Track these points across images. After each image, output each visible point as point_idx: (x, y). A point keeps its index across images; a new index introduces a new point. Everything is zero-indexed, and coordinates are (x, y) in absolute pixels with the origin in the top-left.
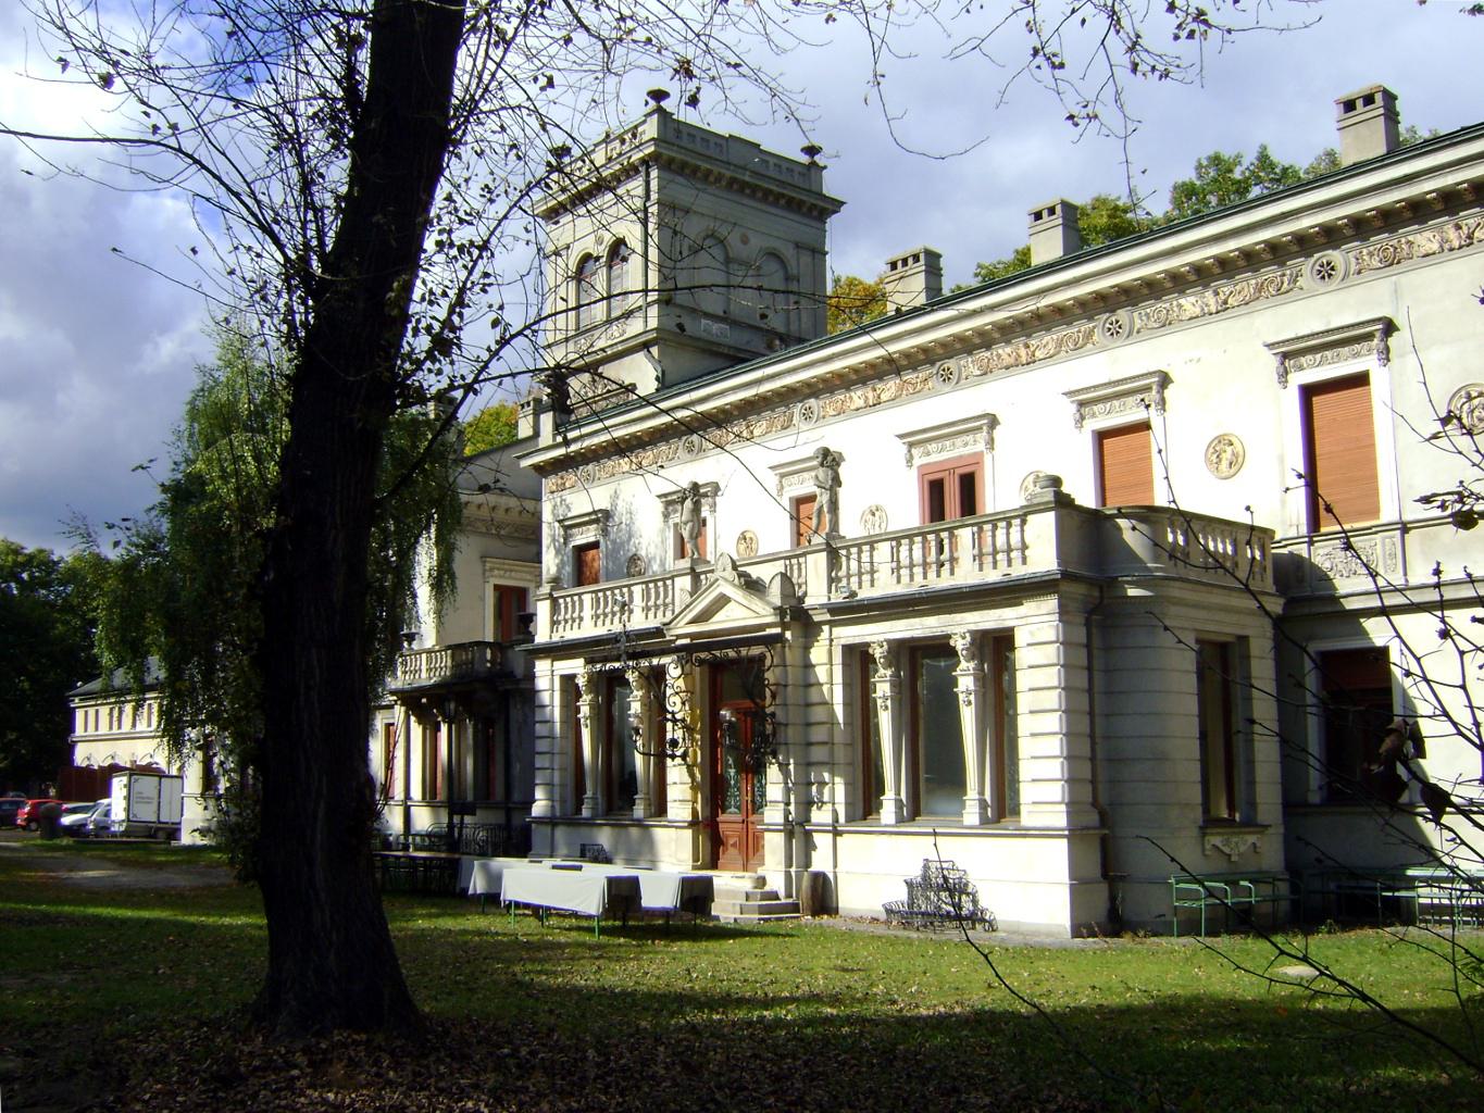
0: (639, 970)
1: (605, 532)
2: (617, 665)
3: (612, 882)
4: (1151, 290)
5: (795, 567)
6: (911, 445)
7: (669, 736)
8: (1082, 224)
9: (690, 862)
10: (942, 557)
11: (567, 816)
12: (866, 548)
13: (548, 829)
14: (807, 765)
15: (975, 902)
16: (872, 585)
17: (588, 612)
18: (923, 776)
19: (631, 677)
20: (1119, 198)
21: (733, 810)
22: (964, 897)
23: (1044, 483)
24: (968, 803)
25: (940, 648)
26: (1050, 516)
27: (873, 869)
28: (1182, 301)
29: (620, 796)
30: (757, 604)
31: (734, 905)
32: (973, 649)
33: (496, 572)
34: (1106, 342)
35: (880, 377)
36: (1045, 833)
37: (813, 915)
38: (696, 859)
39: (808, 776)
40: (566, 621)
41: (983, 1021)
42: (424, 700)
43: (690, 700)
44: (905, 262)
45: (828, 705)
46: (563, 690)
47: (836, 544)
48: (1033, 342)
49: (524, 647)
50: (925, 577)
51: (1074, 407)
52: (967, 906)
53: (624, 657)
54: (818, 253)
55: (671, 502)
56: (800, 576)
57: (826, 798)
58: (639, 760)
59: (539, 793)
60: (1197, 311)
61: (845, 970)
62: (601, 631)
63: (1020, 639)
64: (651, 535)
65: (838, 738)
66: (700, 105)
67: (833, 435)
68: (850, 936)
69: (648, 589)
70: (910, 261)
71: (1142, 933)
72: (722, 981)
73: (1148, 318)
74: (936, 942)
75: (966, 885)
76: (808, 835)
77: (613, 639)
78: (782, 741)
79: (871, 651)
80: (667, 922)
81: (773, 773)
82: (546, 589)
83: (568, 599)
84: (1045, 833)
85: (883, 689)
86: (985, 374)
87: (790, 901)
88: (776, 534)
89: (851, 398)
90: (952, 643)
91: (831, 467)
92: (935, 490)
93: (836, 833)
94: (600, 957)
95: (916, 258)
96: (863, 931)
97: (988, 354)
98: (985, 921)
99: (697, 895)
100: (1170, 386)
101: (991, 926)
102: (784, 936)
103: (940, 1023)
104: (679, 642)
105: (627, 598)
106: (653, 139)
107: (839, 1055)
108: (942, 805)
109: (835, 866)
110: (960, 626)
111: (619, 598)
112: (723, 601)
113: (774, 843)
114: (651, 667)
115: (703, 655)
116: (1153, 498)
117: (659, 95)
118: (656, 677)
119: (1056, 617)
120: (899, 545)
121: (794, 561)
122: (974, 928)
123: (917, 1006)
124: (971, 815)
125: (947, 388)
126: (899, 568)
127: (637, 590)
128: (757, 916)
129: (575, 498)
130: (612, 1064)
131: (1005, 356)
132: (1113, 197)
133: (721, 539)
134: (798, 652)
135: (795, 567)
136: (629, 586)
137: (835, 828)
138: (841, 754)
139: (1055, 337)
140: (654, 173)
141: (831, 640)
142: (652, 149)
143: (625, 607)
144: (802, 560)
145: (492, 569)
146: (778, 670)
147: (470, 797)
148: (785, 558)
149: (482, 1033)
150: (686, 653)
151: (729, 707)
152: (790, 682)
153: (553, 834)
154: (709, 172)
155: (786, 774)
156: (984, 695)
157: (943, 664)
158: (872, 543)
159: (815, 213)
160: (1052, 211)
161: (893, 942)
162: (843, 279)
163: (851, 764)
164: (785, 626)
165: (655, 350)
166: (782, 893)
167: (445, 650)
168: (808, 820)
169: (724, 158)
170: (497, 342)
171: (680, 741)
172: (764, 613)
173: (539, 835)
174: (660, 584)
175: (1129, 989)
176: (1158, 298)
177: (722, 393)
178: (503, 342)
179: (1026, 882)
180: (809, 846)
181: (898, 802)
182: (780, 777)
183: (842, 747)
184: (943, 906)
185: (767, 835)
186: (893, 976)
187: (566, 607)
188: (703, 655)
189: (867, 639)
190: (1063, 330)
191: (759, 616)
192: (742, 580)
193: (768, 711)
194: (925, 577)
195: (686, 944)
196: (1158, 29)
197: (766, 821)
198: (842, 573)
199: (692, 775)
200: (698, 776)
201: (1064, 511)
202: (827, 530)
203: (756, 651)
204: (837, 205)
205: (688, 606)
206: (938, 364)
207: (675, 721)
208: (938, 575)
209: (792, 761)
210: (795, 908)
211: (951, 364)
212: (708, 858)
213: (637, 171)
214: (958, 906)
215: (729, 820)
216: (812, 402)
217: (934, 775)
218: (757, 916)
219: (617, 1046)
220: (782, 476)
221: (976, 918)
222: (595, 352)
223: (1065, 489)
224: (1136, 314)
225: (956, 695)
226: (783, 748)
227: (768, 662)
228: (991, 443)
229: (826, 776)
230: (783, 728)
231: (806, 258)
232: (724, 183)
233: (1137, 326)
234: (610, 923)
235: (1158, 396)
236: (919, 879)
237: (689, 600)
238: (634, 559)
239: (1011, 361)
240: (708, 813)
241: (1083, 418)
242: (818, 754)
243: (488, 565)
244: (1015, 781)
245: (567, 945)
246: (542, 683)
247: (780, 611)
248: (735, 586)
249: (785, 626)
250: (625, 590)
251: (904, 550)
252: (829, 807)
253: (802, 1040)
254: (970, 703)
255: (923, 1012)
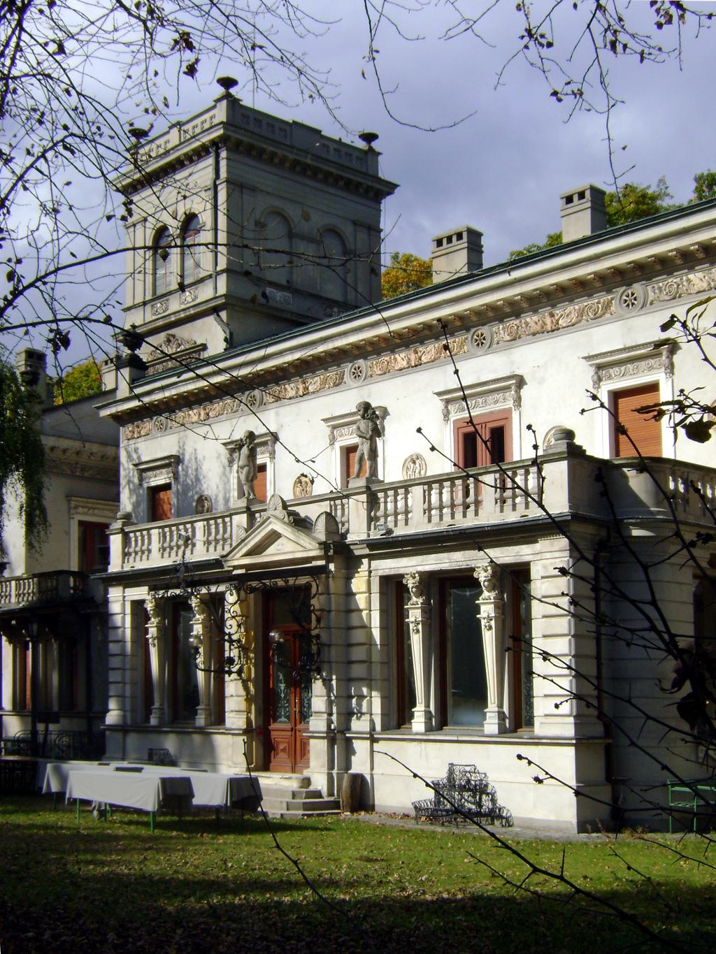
0: (181, 859)
1: (176, 476)
2: (178, 592)
3: (165, 782)
4: (663, 266)
5: (339, 507)
6: (448, 402)
7: (227, 654)
8: (611, 210)
9: (245, 765)
10: (468, 500)
11: (135, 725)
12: (401, 491)
13: (119, 735)
14: (347, 681)
15: (493, 801)
16: (406, 524)
17: (155, 545)
18: (450, 691)
19: (194, 602)
20: (649, 187)
21: (283, 719)
22: (484, 796)
23: (560, 436)
24: (488, 715)
25: (465, 579)
26: (564, 465)
27: (405, 771)
28: (691, 276)
29: (181, 709)
30: (305, 540)
31: (281, 802)
32: (494, 581)
33: (80, 510)
34: (621, 312)
35: (422, 342)
36: (555, 742)
37: (352, 812)
38: (249, 763)
39: (349, 690)
40: (136, 553)
41: (478, 905)
42: (14, 622)
43: (245, 623)
44: (449, 239)
45: (367, 628)
46: (133, 614)
47: (374, 488)
48: (558, 312)
49: (98, 575)
50: (453, 517)
51: (592, 371)
52: (487, 804)
53: (183, 584)
54: (373, 231)
55: (234, 447)
56: (343, 515)
57: (364, 709)
58: (201, 676)
59: (112, 704)
60: (705, 285)
61: (369, 860)
62: (167, 562)
63: (536, 571)
64: (216, 476)
65: (376, 657)
66: (197, 75)
67: (379, 393)
68: (382, 829)
69: (209, 526)
70: (454, 238)
71: (640, 830)
72: (254, 870)
73: (661, 291)
74: (457, 836)
75: (486, 786)
76: (349, 742)
77: (173, 570)
78: (326, 659)
79: (404, 582)
80: (218, 817)
81: (318, 687)
82: (117, 525)
83: (138, 534)
84: (555, 742)
85: (415, 614)
86: (515, 339)
87: (332, 799)
88: (329, 475)
89: (395, 359)
90: (475, 575)
91: (372, 420)
92: (468, 443)
93: (373, 740)
94: (150, 848)
95: (459, 236)
96: (397, 826)
97: (517, 322)
98: (502, 817)
99: (245, 795)
100: (679, 352)
101: (508, 822)
102: (322, 830)
103: (441, 907)
104: (235, 572)
105: (190, 534)
106: (222, 123)
107: (340, 937)
108: (466, 716)
109: (372, 768)
110: (479, 562)
111: (183, 533)
112: (274, 536)
113: (318, 748)
114: (211, 595)
115: (254, 584)
116: (660, 450)
117: (228, 83)
118: (215, 604)
119: (567, 553)
120: (430, 489)
121: (338, 502)
122: (493, 824)
123: (424, 893)
124: (491, 725)
125: (480, 351)
126: (430, 509)
127: (200, 526)
128: (301, 812)
129: (146, 446)
130: (130, 946)
131: (532, 324)
132: (642, 187)
133: (280, 480)
134: (341, 582)
135: (339, 507)
136: (192, 523)
137: (372, 735)
138: (377, 671)
139: (577, 307)
140: (224, 154)
141: (370, 572)
142: (221, 132)
143: (188, 541)
144: (345, 501)
145: (76, 507)
146: (322, 597)
147: (56, 708)
148: (330, 499)
149: (11, 918)
150: (240, 582)
151: (277, 629)
152: (333, 607)
153: (124, 743)
154: (273, 155)
155: (329, 688)
156: (504, 621)
157: (468, 593)
158: (406, 486)
159: (371, 194)
160: (581, 195)
161: (419, 835)
162: (400, 256)
163: (387, 680)
164: (329, 559)
165: (223, 314)
166: (325, 791)
167: (32, 578)
168: (348, 729)
169: (288, 143)
170: (12, 293)
171: (236, 659)
172: (311, 547)
173: (113, 740)
174: (220, 521)
175: (617, 879)
176: (670, 274)
177: (280, 353)
178: (16, 293)
179: (536, 783)
180: (349, 751)
181: (428, 713)
182: (324, 691)
183: (379, 665)
184: (462, 805)
185: (312, 741)
186: (411, 866)
187: (136, 541)
188: (254, 584)
189: (401, 571)
190: (584, 301)
191: (306, 550)
192: (291, 518)
193: (314, 633)
194: (453, 517)
195: (232, 837)
196: (640, 18)
197: (310, 729)
198: (381, 513)
199: (246, 688)
200: (252, 689)
201: (576, 461)
202: (367, 475)
203: (303, 580)
204: (390, 188)
205: (243, 541)
206: (473, 330)
207: (231, 641)
208: (465, 516)
209: (334, 677)
210: (336, 805)
211: (485, 330)
212: (261, 763)
213: (208, 153)
214: (479, 805)
215: (280, 728)
216: (361, 362)
217: (460, 693)
218: (301, 812)
219: (137, 929)
220: (334, 427)
221: (495, 814)
222: (169, 315)
223: (577, 441)
224: (649, 288)
225: (479, 621)
226: (325, 666)
227: (314, 590)
228: (518, 401)
229: (365, 690)
230: (326, 648)
231: (362, 235)
232: (287, 165)
233: (650, 299)
234: (168, 818)
235: (667, 362)
236: (445, 781)
237: (244, 535)
238: (202, 499)
239: (538, 328)
240: (261, 722)
241: (600, 379)
242: (358, 671)
243: (73, 504)
244: (530, 696)
245: (123, 837)
246: (115, 607)
247: (324, 546)
248: (285, 523)
249: (329, 559)
250: (189, 526)
251: (434, 493)
252: (367, 717)
253: (309, 923)
254: (490, 628)
255: (428, 897)
